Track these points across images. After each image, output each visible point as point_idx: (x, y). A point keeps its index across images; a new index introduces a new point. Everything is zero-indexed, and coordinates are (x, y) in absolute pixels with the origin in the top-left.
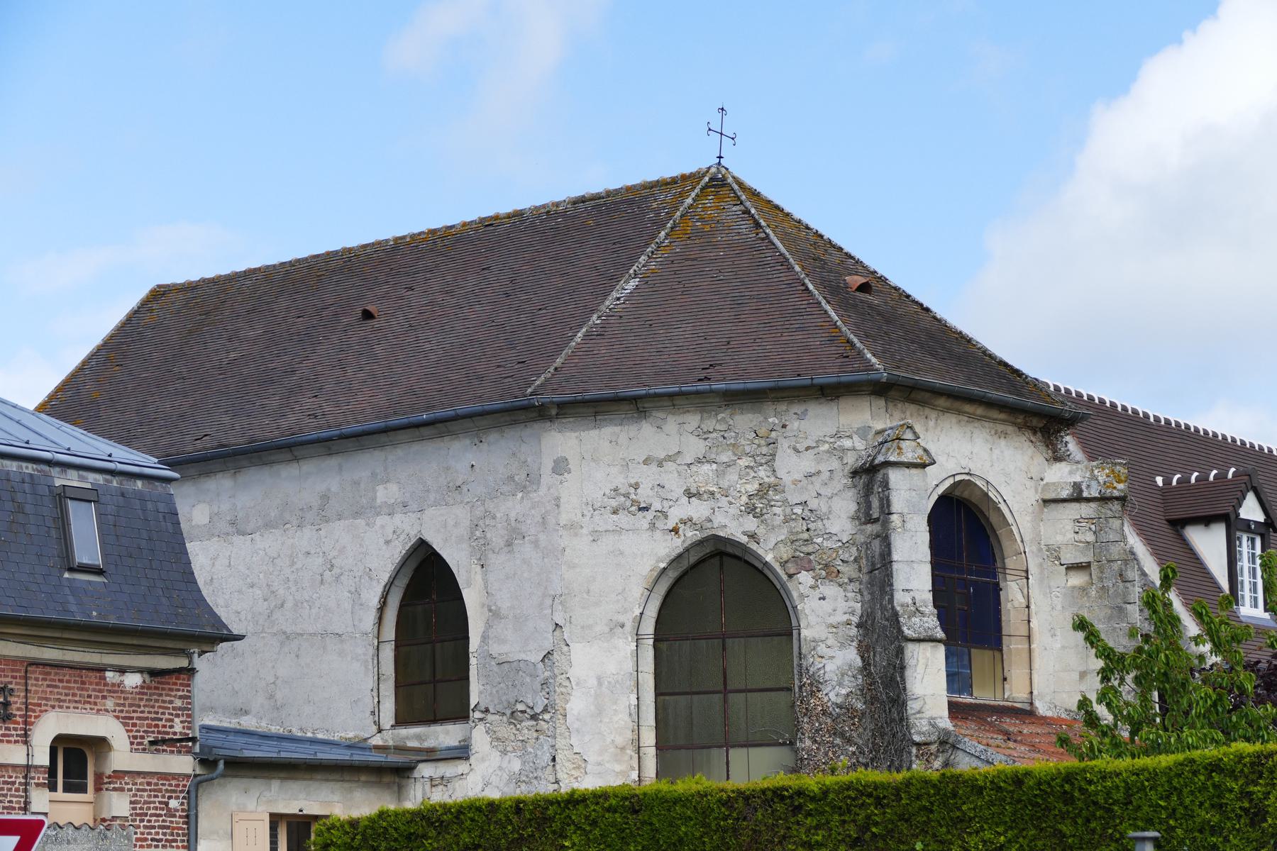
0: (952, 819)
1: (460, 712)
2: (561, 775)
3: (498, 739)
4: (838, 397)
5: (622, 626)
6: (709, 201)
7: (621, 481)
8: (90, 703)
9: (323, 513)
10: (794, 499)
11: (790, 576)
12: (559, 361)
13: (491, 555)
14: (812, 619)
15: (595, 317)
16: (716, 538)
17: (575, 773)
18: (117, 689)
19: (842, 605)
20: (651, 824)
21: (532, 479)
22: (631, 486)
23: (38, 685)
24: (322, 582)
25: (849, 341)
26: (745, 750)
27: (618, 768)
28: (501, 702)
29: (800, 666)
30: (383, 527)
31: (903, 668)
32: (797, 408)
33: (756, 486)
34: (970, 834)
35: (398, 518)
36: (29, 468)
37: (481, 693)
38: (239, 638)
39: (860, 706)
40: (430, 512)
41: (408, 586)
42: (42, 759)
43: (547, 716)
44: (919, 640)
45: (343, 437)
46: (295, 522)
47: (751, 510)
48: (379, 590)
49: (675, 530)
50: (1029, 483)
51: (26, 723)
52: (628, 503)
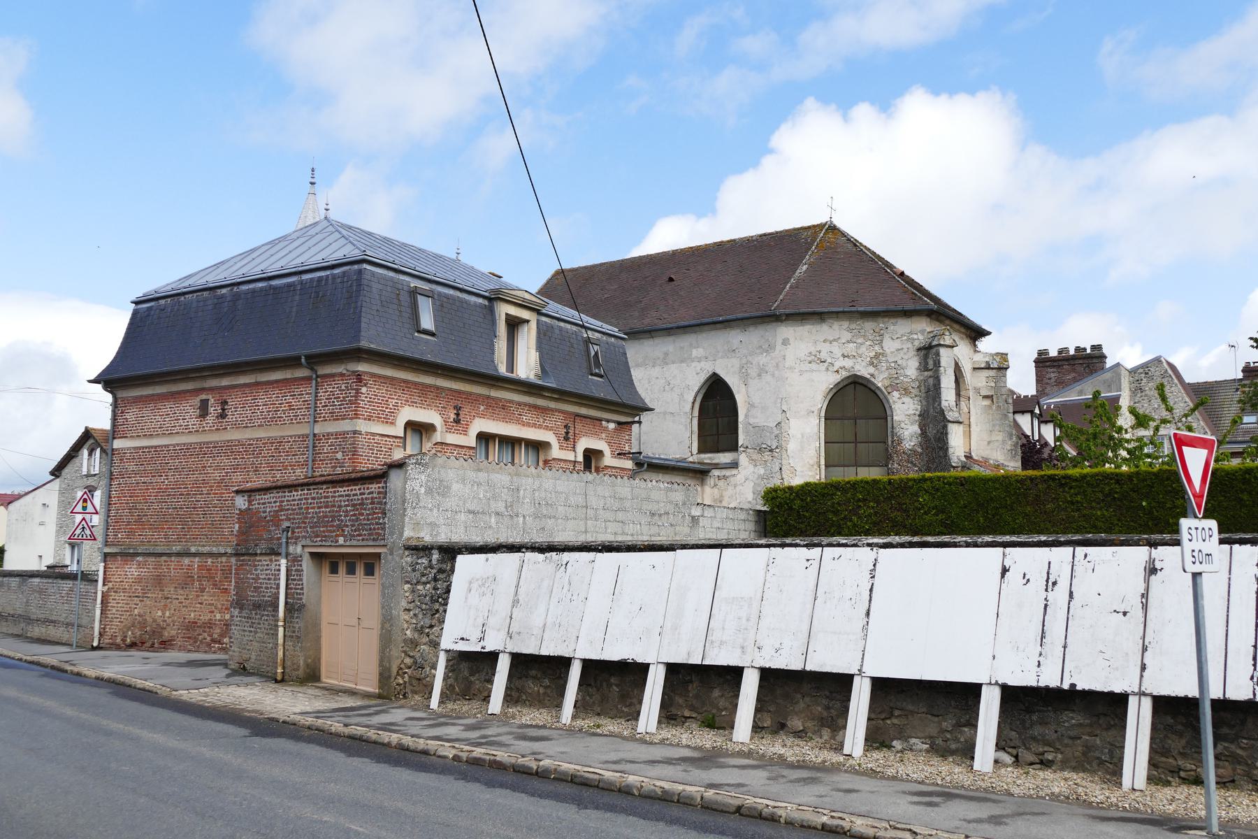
0: (1166, 492)
1: (734, 447)
2: (784, 476)
3: (753, 460)
4: (911, 316)
5: (813, 412)
6: (830, 235)
7: (813, 349)
8: (596, 435)
9: (666, 360)
10: (891, 360)
11: (889, 393)
12: (781, 297)
13: (749, 380)
14: (898, 412)
15: (792, 280)
16: (855, 375)
17: (791, 475)
18: (606, 429)
19: (912, 407)
20: (974, 491)
21: (771, 347)
22: (817, 351)
23: (579, 426)
24: (664, 390)
25: (913, 293)
26: (867, 468)
27: (810, 474)
28: (754, 444)
29: (892, 432)
30: (695, 367)
31: (947, 434)
32: (893, 320)
33: (874, 354)
34: (1178, 499)
35: (703, 364)
36: (575, 328)
37: (744, 440)
38: (652, 410)
39: (920, 450)
40: (717, 362)
41: (705, 393)
42: (580, 458)
43: (777, 450)
44: (953, 422)
45: (678, 328)
46: (651, 364)
47: (872, 364)
48: (693, 394)
49: (837, 372)
50: (970, 360)
51: (574, 442)
52: (816, 359)
